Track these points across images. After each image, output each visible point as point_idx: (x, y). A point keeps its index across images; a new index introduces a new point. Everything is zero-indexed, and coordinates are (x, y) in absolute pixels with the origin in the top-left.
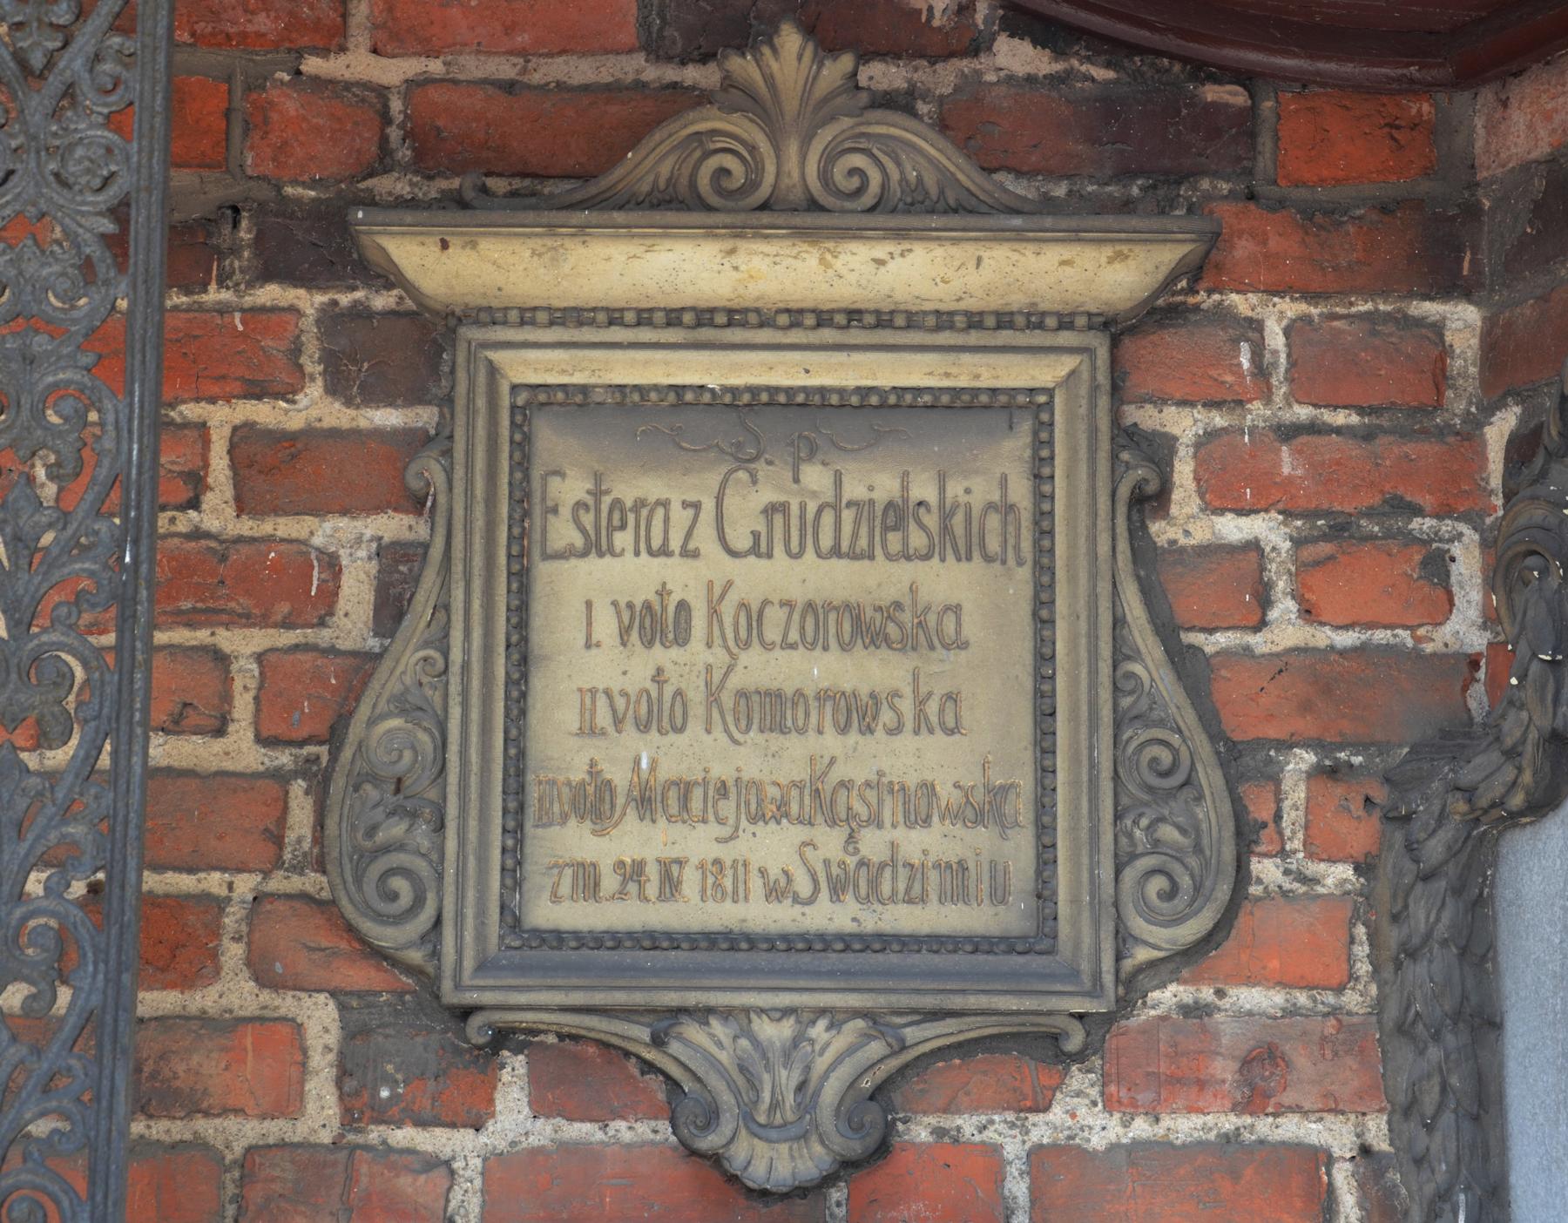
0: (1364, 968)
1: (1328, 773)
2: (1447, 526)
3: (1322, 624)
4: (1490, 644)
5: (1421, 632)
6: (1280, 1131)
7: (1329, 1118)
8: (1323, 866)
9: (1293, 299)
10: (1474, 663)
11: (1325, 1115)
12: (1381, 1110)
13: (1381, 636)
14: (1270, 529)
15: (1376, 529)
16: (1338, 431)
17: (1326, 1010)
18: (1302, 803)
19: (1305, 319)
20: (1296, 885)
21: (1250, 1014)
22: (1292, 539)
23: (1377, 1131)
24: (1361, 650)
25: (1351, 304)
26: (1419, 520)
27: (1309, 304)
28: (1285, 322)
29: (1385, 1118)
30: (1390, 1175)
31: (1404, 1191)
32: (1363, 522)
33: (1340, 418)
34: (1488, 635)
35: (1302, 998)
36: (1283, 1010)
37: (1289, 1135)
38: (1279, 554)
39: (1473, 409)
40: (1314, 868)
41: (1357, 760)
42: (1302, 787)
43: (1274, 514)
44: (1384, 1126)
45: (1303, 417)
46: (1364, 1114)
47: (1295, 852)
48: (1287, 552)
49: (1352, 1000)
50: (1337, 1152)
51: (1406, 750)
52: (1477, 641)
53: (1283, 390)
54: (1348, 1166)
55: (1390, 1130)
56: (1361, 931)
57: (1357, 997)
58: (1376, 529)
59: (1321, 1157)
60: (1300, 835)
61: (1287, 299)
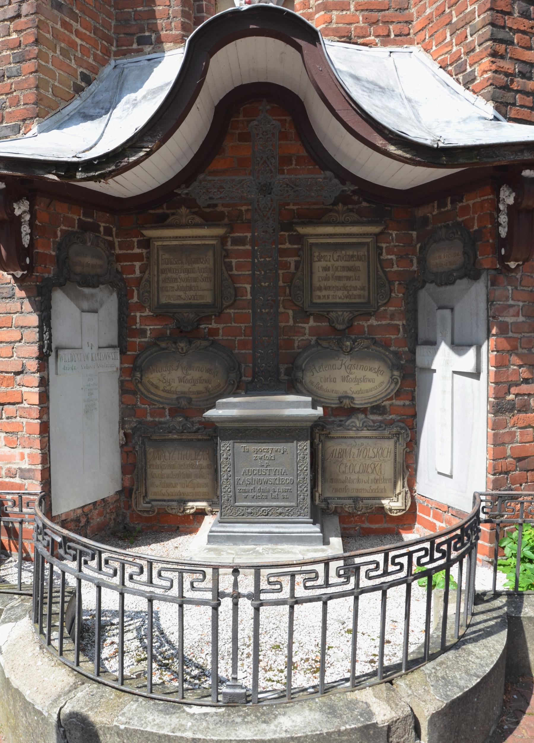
23: (404, 322)
49: (402, 308)
52: (416, 269)
59: (399, 325)
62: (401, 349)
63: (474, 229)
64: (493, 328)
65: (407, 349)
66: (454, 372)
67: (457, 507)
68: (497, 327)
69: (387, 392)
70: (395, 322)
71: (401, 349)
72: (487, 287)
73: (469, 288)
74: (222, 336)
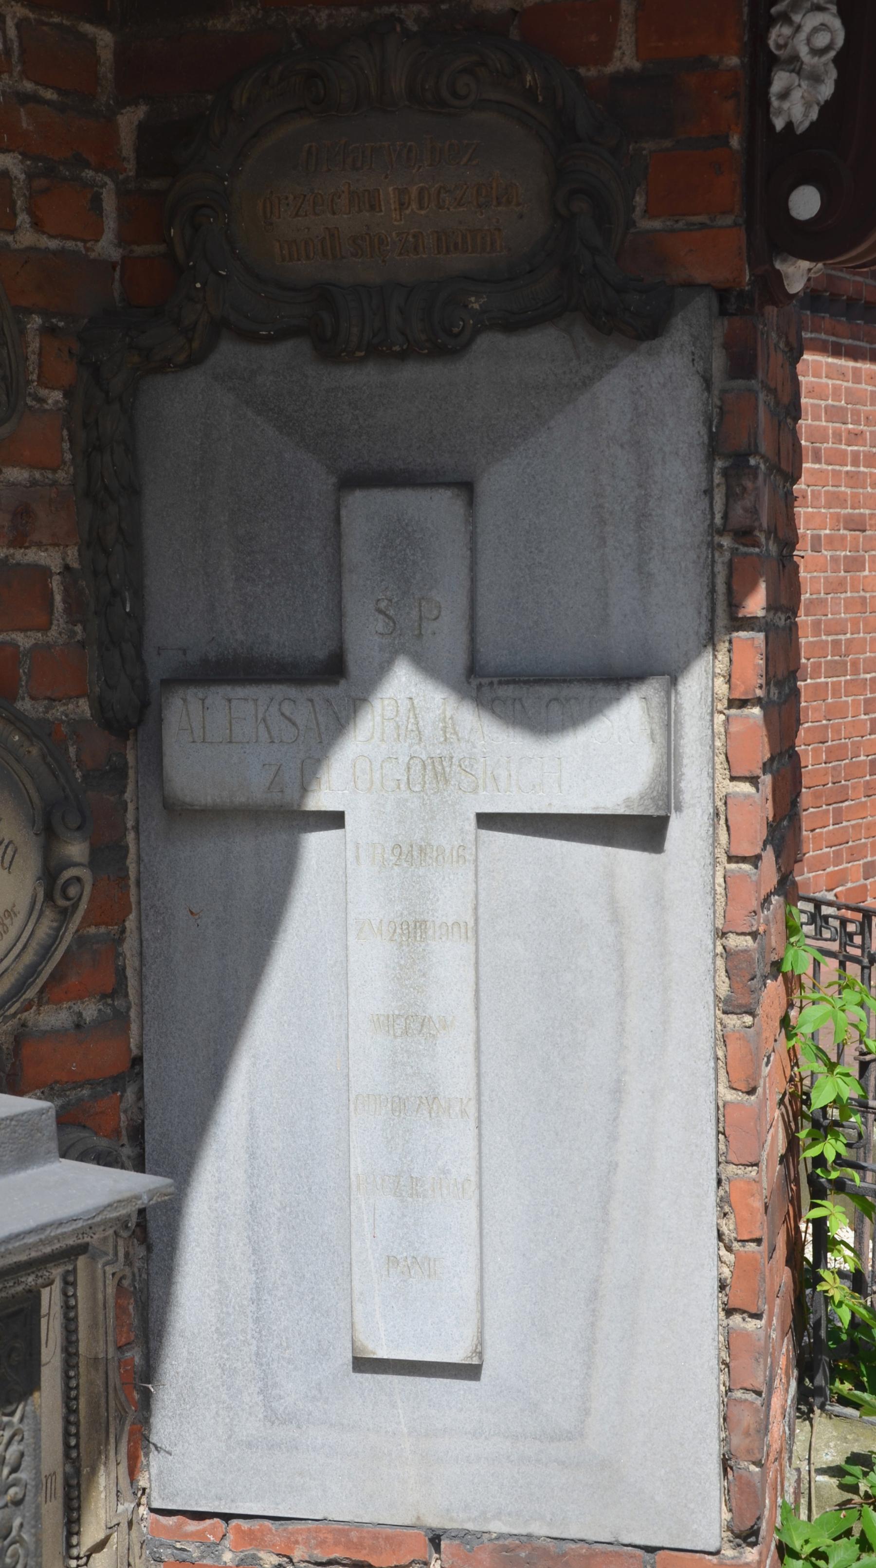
0: (68, 456)
1: (48, 331)
2: (100, 177)
3: (44, 233)
4: (123, 258)
5: (89, 245)
6: (27, 558)
7: (51, 548)
8: (47, 391)
9: (23, 5)
10: (114, 266)
11: (48, 547)
12: (75, 545)
13: (70, 244)
14: (14, 164)
15: (67, 173)
16: (48, 103)
17: (50, 482)
18: (37, 350)
19: (26, 19)
20: (34, 403)
21: (13, 484)
22: (26, 173)
23: (72, 553)
24: (60, 253)
25: (52, 16)
26: (87, 171)
27: (30, 11)
28: (16, 20)
29: (76, 548)
30: (80, 582)
31: (87, 592)
32: (61, 168)
33: (50, 95)
34: (121, 250)
35: (37, 475)
36: (30, 481)
37: (31, 559)
38: (19, 181)
39: (111, 102)
40: (43, 392)
41: (61, 324)
42: (37, 340)
43: (16, 154)
44: (76, 553)
45: (29, 90)
46: (67, 546)
47: (33, 381)
48: (24, 181)
49: (61, 475)
50: (54, 569)
51: (86, 321)
52: (115, 254)
53: (19, 68)
54: (58, 577)
55: (80, 555)
56: (65, 433)
57: (64, 475)
58: (67, 173)
59: (45, 572)
60: (36, 371)
61: (19, 4)
62: (58, 711)
63: (613, 67)
64: (752, 587)
65: (84, 708)
66: (487, 821)
67: (497, 1527)
68: (766, 581)
69: (20, 967)
70: (33, 556)
71: (58, 711)
72: (707, 383)
73: (587, 383)
74: (852, 634)
